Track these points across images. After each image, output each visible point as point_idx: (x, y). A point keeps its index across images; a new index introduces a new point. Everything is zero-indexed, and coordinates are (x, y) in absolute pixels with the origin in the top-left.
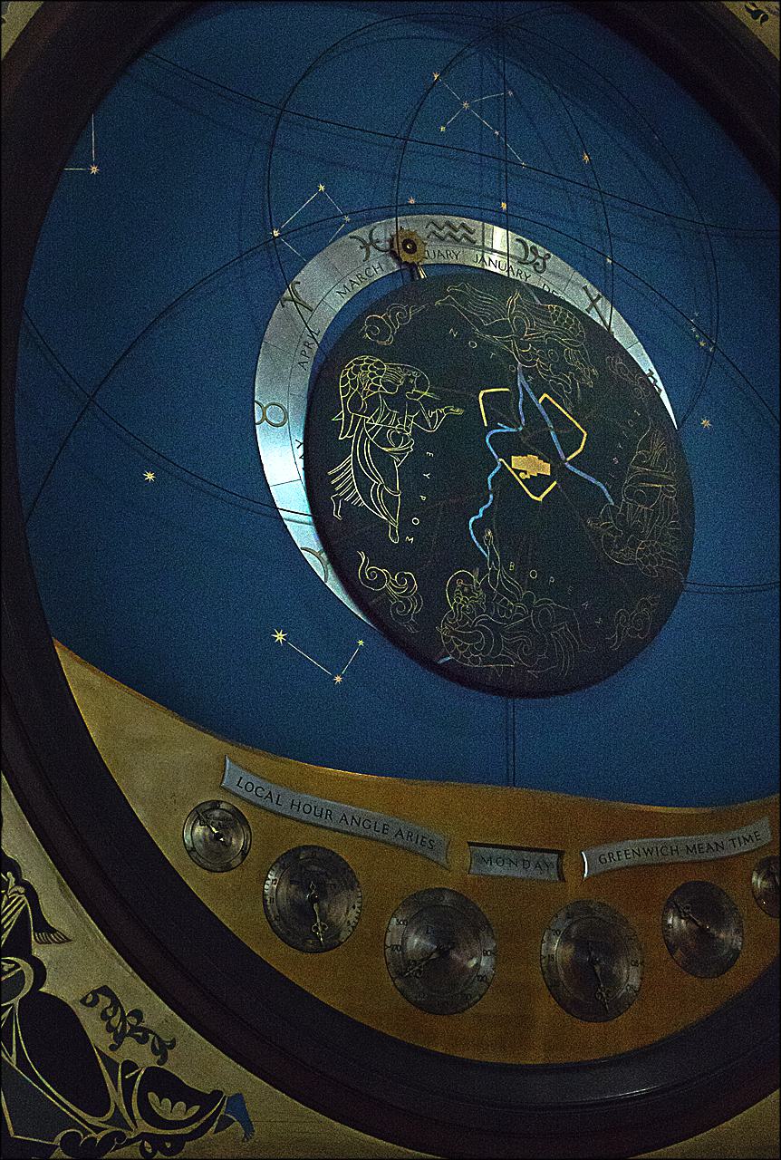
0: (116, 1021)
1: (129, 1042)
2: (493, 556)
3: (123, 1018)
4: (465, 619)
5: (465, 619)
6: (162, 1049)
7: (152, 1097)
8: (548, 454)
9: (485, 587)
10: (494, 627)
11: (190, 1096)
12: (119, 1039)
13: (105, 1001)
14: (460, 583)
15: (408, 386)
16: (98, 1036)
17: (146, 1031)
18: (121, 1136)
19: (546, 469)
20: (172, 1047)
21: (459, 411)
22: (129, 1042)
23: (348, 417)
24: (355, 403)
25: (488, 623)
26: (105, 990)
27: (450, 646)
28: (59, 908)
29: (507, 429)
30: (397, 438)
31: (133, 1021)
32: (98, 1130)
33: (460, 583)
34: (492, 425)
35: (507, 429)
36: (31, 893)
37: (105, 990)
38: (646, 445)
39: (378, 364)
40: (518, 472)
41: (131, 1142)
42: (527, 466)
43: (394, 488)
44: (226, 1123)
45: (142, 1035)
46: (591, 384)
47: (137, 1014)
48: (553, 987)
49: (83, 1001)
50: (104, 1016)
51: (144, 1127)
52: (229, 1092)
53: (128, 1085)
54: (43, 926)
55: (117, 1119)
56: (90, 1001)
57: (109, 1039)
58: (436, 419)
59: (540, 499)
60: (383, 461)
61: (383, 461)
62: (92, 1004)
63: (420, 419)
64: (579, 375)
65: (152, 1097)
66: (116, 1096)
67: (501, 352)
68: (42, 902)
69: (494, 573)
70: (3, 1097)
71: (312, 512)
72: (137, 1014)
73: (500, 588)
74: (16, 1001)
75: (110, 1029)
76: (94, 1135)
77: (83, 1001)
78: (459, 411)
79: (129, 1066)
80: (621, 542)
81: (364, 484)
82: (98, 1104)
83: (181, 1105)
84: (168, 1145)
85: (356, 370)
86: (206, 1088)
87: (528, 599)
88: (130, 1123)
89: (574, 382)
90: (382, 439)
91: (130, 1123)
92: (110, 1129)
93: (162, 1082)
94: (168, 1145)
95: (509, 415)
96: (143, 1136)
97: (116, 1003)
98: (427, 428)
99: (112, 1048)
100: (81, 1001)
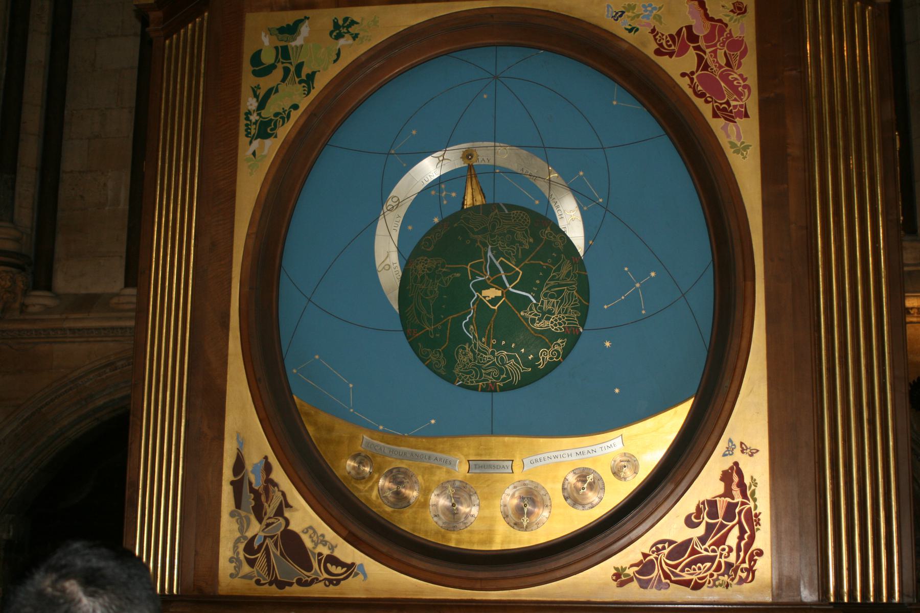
0: (315, 538)
2: (474, 337)
6: (332, 548)
7: (329, 565)
8: (499, 284)
9: (472, 351)
12: (316, 545)
15: (437, 267)
16: (308, 544)
17: (326, 542)
18: (317, 579)
19: (499, 293)
25: (475, 365)
26: (311, 528)
29: (481, 279)
35: (481, 279)
36: (284, 494)
37: (311, 528)
40: (485, 297)
44: (357, 574)
45: (325, 543)
46: (527, 247)
47: (323, 535)
48: (506, 516)
50: (310, 537)
51: (326, 576)
53: (319, 562)
55: (316, 572)
56: (305, 531)
62: (306, 533)
65: (329, 565)
66: (315, 565)
68: (124, 204)
69: (475, 344)
71: (447, 218)
72: (323, 535)
75: (313, 541)
77: (747, 116)
79: (320, 554)
82: (309, 568)
83: (339, 568)
86: (349, 561)
87: (493, 353)
93: (333, 560)
96: (325, 579)
97: (315, 532)
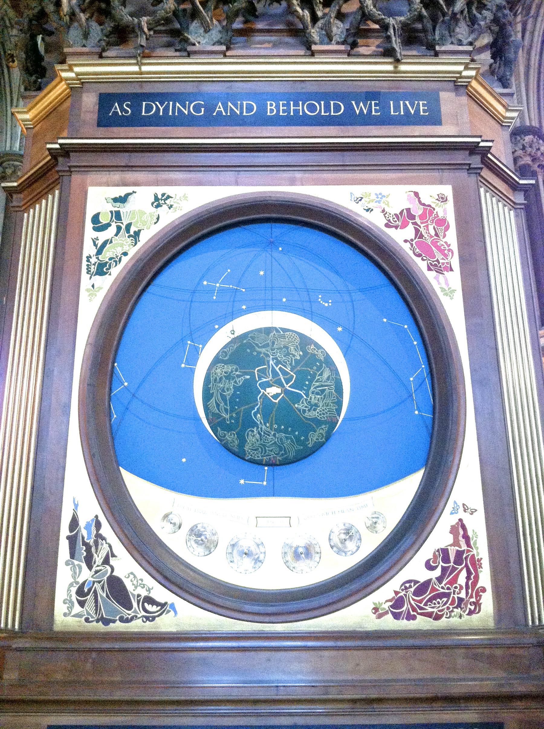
0: (135, 582)
1: (139, 588)
2: (261, 423)
3: (137, 581)
4: (253, 444)
5: (253, 444)
6: (149, 590)
7: (146, 604)
10: (264, 445)
11: (157, 604)
12: (136, 587)
13: (132, 576)
14: (250, 433)
15: (232, 371)
16: (130, 587)
18: (136, 617)
19: (279, 390)
20: (152, 589)
21: (248, 377)
22: (139, 588)
23: (213, 385)
24: (215, 380)
25: (261, 444)
27: (249, 453)
28: (119, 548)
30: (228, 390)
31: (140, 582)
32: (129, 615)
33: (250, 433)
34: (260, 379)
36: (110, 546)
37: (132, 573)
38: (321, 374)
39: (223, 366)
40: (268, 394)
41: (139, 618)
42: (273, 391)
43: (227, 406)
46: (298, 358)
47: (142, 580)
49: (451, 270)
50: (131, 581)
52: (169, 603)
53: (138, 602)
54: (113, 556)
55: (135, 611)
57: (133, 587)
58: (240, 381)
59: (277, 401)
60: (223, 397)
61: (223, 397)
62: (128, 578)
63: (235, 382)
64: (294, 356)
65: (146, 604)
66: (135, 604)
67: (264, 354)
69: (261, 428)
70: (434, 248)
73: (264, 433)
74: (105, 578)
75: (133, 584)
76: (128, 616)
78: (248, 377)
80: (309, 410)
81: (218, 405)
82: (129, 607)
84: (151, 619)
85: (216, 369)
86: (163, 602)
88: (139, 612)
89: (292, 359)
90: (223, 391)
91: (139, 612)
92: (133, 614)
93: (150, 600)
94: (151, 619)
95: (266, 375)
96: (143, 616)
97: (135, 577)
98: (237, 384)
99: (134, 590)
100: (99, 125)
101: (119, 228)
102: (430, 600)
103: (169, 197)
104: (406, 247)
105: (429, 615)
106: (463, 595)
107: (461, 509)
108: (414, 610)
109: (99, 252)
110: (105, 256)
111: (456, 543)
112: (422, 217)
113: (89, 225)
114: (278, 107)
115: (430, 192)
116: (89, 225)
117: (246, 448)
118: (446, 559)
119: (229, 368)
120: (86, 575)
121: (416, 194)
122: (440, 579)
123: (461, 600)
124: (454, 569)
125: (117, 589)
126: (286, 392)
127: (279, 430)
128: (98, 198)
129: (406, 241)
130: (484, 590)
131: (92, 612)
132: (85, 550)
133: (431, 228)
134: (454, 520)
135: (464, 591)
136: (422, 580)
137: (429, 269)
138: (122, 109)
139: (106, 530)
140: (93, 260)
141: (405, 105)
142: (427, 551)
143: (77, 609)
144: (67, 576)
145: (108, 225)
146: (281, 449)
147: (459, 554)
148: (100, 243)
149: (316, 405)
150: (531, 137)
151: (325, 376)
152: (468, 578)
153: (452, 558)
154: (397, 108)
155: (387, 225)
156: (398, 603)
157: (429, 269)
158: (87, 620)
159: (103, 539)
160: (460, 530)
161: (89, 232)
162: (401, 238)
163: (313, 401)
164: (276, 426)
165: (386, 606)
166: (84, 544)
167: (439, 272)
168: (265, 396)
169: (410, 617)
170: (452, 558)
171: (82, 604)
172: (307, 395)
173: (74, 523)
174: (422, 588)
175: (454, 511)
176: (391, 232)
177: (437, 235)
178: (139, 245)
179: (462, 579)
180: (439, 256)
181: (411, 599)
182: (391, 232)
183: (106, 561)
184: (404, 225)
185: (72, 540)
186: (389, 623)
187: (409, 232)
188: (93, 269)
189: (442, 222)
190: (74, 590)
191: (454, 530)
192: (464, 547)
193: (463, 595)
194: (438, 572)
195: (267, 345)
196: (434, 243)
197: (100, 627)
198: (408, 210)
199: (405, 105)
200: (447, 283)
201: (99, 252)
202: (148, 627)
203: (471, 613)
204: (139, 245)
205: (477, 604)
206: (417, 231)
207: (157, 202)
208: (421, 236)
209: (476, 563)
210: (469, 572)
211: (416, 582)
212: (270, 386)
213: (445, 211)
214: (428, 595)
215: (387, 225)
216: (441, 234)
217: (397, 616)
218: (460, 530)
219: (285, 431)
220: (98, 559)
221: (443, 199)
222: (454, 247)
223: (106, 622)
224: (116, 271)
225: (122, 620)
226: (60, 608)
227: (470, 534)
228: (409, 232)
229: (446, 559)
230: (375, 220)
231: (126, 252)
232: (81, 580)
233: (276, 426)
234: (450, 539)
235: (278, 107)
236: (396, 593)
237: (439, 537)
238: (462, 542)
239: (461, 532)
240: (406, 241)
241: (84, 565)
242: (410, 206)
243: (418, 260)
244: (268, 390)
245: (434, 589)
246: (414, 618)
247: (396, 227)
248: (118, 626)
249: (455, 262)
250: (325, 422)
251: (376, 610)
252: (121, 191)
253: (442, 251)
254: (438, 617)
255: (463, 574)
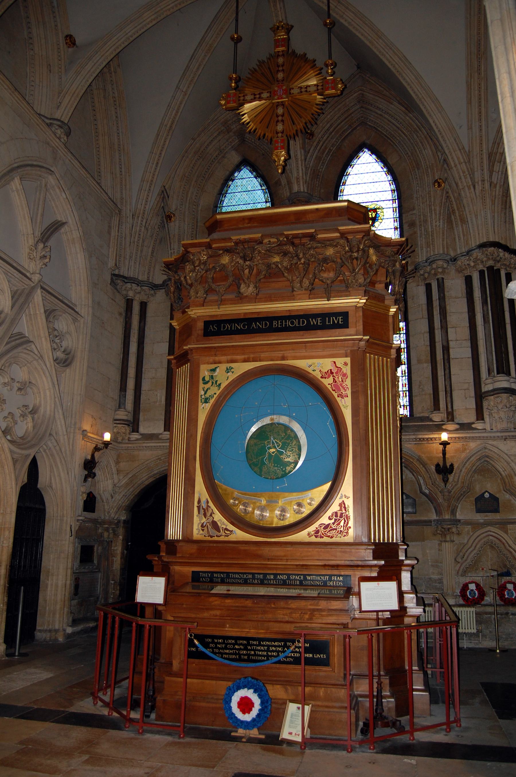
6: (226, 526)
16: (219, 525)
19: (275, 450)
66: (221, 531)
82: (220, 532)
93: (226, 529)
101: (213, 383)
102: (329, 531)
103: (232, 368)
104: (329, 387)
105: (329, 536)
106: (342, 529)
107: (344, 497)
108: (323, 534)
109: (205, 393)
110: (209, 393)
111: (341, 510)
112: (337, 373)
113: (201, 382)
114: (278, 323)
115: (340, 361)
116: (201, 382)
117: (262, 473)
118: (336, 516)
119: (255, 441)
120: (204, 520)
121: (335, 362)
122: (333, 523)
123: (341, 531)
124: (339, 519)
125: (215, 525)
126: (277, 451)
127: (274, 466)
128: (204, 371)
129: (329, 384)
130: (350, 528)
131: (207, 533)
132: (205, 512)
133: (340, 377)
134: (341, 501)
135: (342, 528)
136: (327, 524)
137: (338, 397)
138: (214, 328)
139: (211, 504)
140: (203, 397)
141: (333, 319)
142: (329, 513)
143: (201, 532)
144: (197, 520)
145: (208, 381)
146: (276, 473)
147: (342, 514)
148: (205, 389)
149: (289, 456)
150: (492, 248)
151: (294, 444)
152: (344, 523)
153: (339, 515)
154: (329, 321)
155: (322, 377)
156: (317, 532)
157: (338, 397)
158: (205, 536)
159: (210, 507)
160: (342, 505)
161: (201, 385)
162: (327, 382)
163: (288, 454)
164: (273, 465)
165: (313, 533)
166: (203, 509)
167: (342, 398)
168: (269, 453)
169: (321, 537)
170: (339, 515)
171: (203, 530)
172: (286, 452)
173: (199, 501)
174: (327, 526)
175: (341, 497)
176: (323, 380)
177: (342, 381)
178: (221, 389)
179: (342, 524)
180: (342, 390)
181: (322, 530)
182: (323, 380)
183: (211, 515)
184: (329, 377)
185: (199, 507)
186: (313, 539)
187: (331, 380)
188: (203, 401)
189: (345, 375)
190: (200, 525)
191: (340, 505)
192: (344, 511)
193: (342, 529)
194: (333, 521)
195: (270, 431)
196: (341, 385)
197: (209, 539)
198: (331, 370)
199: (333, 319)
200: (345, 403)
201: (205, 393)
202: (226, 539)
203: (345, 536)
204: (221, 389)
205: (347, 533)
206: (334, 379)
207: (228, 370)
208: (336, 382)
209: (348, 517)
210: (345, 521)
211: (324, 524)
212: (271, 448)
213: (346, 370)
214: (328, 529)
215: (322, 377)
216: (344, 381)
217: (316, 537)
218: (342, 505)
219: (277, 466)
220: (208, 514)
221: (346, 364)
222: (349, 386)
223: (211, 537)
224: (212, 401)
225: (217, 536)
226: (195, 532)
227: (346, 506)
228: (331, 380)
229: (336, 516)
230: (318, 375)
231: (215, 392)
232: (202, 522)
233: (273, 465)
234: (339, 508)
235: (278, 323)
236: (317, 528)
237: (334, 507)
238: (343, 509)
239: (343, 506)
240: (329, 384)
241: (203, 517)
242: (332, 368)
243: (333, 392)
244: (270, 450)
245: (331, 527)
246: (323, 537)
247: (325, 378)
248: (216, 538)
249: (349, 392)
250: (293, 463)
251: (309, 534)
252: (213, 366)
253: (344, 388)
254: (332, 537)
255: (343, 521)
